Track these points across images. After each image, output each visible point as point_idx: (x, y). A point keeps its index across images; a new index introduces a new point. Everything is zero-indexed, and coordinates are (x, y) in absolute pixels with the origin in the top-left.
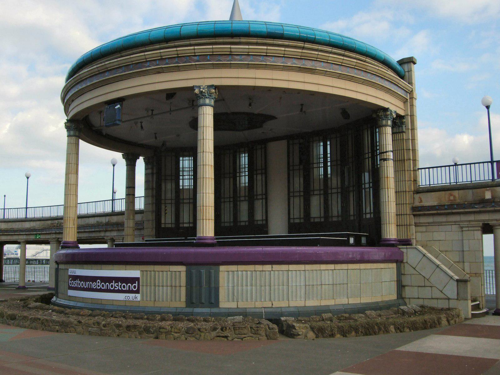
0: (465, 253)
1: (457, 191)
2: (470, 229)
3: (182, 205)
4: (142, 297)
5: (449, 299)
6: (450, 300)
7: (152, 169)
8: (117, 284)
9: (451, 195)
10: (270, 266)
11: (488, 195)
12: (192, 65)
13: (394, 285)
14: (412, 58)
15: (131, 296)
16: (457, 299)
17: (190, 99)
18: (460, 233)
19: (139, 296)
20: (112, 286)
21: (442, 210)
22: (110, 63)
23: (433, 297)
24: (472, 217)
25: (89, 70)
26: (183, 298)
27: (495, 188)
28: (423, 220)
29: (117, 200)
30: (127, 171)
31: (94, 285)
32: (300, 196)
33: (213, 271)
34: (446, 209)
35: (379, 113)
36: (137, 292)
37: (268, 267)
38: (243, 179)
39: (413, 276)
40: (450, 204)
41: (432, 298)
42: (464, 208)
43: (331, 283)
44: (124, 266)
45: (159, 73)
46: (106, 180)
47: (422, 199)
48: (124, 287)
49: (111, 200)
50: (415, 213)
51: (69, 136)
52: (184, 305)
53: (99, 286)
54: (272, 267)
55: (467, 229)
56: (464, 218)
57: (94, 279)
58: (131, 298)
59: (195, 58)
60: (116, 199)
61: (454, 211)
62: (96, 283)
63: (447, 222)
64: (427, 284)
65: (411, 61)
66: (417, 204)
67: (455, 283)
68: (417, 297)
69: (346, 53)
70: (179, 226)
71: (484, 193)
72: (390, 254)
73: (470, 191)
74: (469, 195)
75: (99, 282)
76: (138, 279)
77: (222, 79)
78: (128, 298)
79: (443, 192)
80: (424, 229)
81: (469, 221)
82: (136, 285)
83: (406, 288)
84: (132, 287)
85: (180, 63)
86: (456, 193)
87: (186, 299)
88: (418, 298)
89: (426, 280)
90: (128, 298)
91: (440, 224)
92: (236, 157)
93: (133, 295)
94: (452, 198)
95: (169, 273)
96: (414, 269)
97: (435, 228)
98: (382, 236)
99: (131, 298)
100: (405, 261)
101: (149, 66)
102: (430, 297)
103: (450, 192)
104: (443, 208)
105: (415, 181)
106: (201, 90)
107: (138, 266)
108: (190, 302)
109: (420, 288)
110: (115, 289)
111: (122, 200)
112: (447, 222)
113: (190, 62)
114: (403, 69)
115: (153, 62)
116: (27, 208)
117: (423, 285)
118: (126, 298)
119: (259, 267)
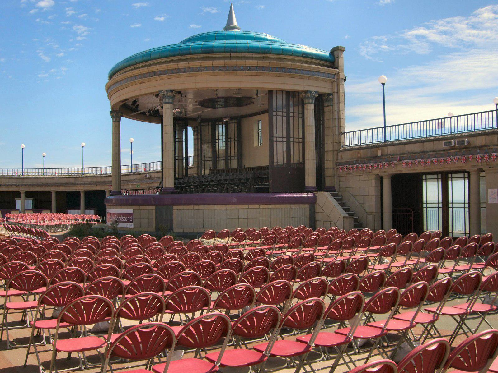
3: (236, 155)
7: (197, 135)
10: (203, 206)
15: (130, 224)
19: (133, 224)
25: (120, 73)
26: (154, 226)
27: (382, 148)
29: (389, 128)
30: (113, 147)
32: (223, 160)
36: (132, 222)
37: (201, 207)
38: (221, 144)
43: (246, 217)
44: (125, 207)
46: (145, 148)
49: (382, 127)
51: (113, 121)
54: (204, 207)
59: (159, 72)
60: (347, 133)
64: (328, 219)
70: (236, 169)
71: (377, 151)
72: (6, 235)
74: (369, 153)
82: (132, 218)
83: (318, 222)
84: (130, 220)
86: (361, 151)
92: (216, 130)
94: (359, 156)
96: (322, 208)
98: (306, 184)
100: (317, 202)
103: (357, 151)
105: (339, 142)
111: (350, 133)
116: (385, 127)
119: (196, 207)
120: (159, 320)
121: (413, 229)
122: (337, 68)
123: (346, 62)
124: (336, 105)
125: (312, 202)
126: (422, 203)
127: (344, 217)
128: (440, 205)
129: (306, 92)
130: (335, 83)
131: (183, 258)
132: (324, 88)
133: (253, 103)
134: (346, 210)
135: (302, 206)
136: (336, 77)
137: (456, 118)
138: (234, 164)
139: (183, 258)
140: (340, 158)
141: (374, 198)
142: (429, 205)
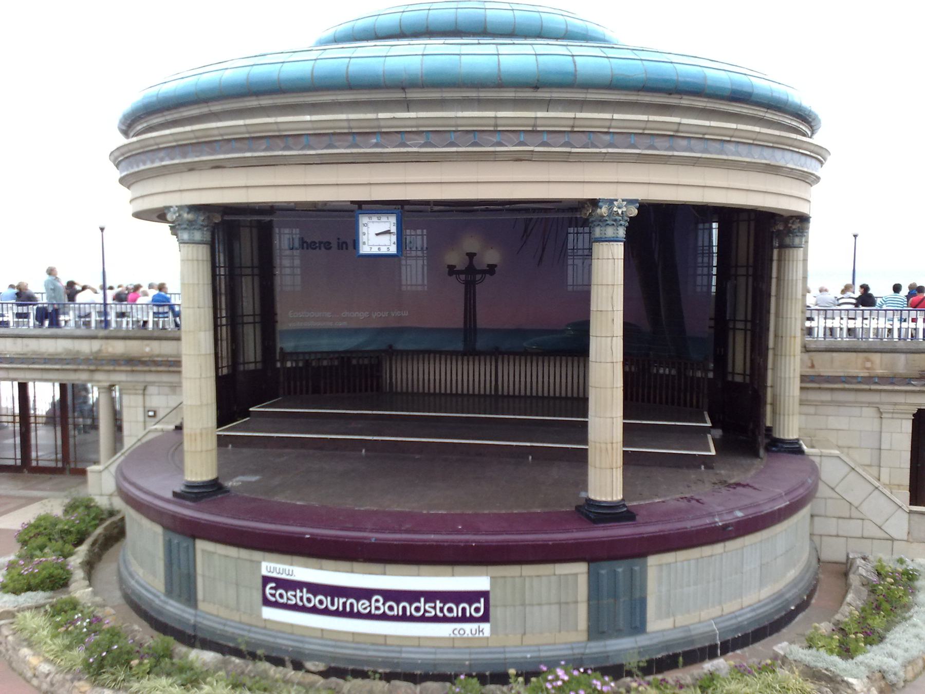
0: (884, 453)
1: (879, 355)
2: (895, 416)
4: (493, 630)
5: (893, 540)
6: (895, 543)
8: (433, 605)
9: (868, 360)
12: (601, 153)
14: (815, 118)
16: (907, 541)
17: (578, 216)
18: (877, 421)
19: (486, 627)
20: (417, 609)
21: (851, 383)
22: (394, 118)
23: (865, 535)
24: (900, 399)
26: (583, 624)
31: (362, 606)
33: (637, 568)
34: (859, 383)
35: (793, 223)
36: (485, 618)
39: (829, 501)
40: (867, 375)
41: (863, 538)
42: (892, 384)
44: (448, 569)
45: (191, 170)
47: (815, 363)
48: (450, 610)
50: (804, 385)
52: (583, 636)
53: (377, 608)
55: (890, 416)
56: (885, 398)
57: (412, 596)
58: (468, 632)
59: (607, 138)
61: (873, 387)
62: (370, 602)
63: (856, 402)
64: (855, 514)
67: (907, 516)
68: (834, 533)
69: (768, 115)
73: (902, 357)
75: (377, 601)
76: (485, 594)
77: (651, 187)
78: (462, 632)
79: (854, 354)
80: (812, 410)
81: (895, 404)
84: (470, 611)
85: (574, 145)
86: (876, 357)
87: (589, 627)
88: (837, 536)
89: (853, 508)
90: (462, 632)
91: (840, 404)
93: (474, 626)
94: (868, 365)
95: (553, 579)
97: (831, 410)
99: (468, 632)
101: (500, 144)
102: (860, 535)
104: (855, 381)
106: (615, 209)
107: (483, 569)
108: (596, 631)
109: (840, 521)
110: (427, 615)
112: (856, 402)
113: (597, 147)
115: (511, 135)
117: (848, 516)
118: (456, 632)
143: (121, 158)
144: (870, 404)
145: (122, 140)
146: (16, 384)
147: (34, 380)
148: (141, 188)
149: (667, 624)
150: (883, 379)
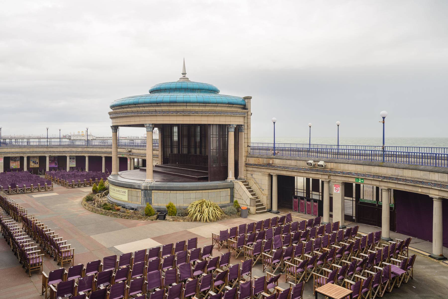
11: (271, 162)
13: (229, 198)
24: (265, 170)
28: (249, 169)
56: (262, 170)
65: (249, 98)
66: (247, 162)
86: (260, 159)
114: (243, 106)
120: (25, 160)
121: (142, 152)
122: (246, 109)
123: (253, 106)
124: (246, 130)
125: (232, 188)
126: (295, 189)
127: (250, 199)
128: (305, 191)
129: (230, 125)
130: (246, 118)
131: (87, 170)
132: (238, 121)
133: (112, 107)
134: (253, 195)
135: (226, 190)
136: (246, 114)
137: (418, 148)
138: (185, 151)
139: (87, 170)
140: (247, 160)
141: (267, 186)
142: (298, 190)
143: (110, 114)
144: (260, 172)
145: (111, 110)
146: (305, 179)
147: (297, 176)
148: (115, 120)
149: (157, 205)
150: (260, 165)
